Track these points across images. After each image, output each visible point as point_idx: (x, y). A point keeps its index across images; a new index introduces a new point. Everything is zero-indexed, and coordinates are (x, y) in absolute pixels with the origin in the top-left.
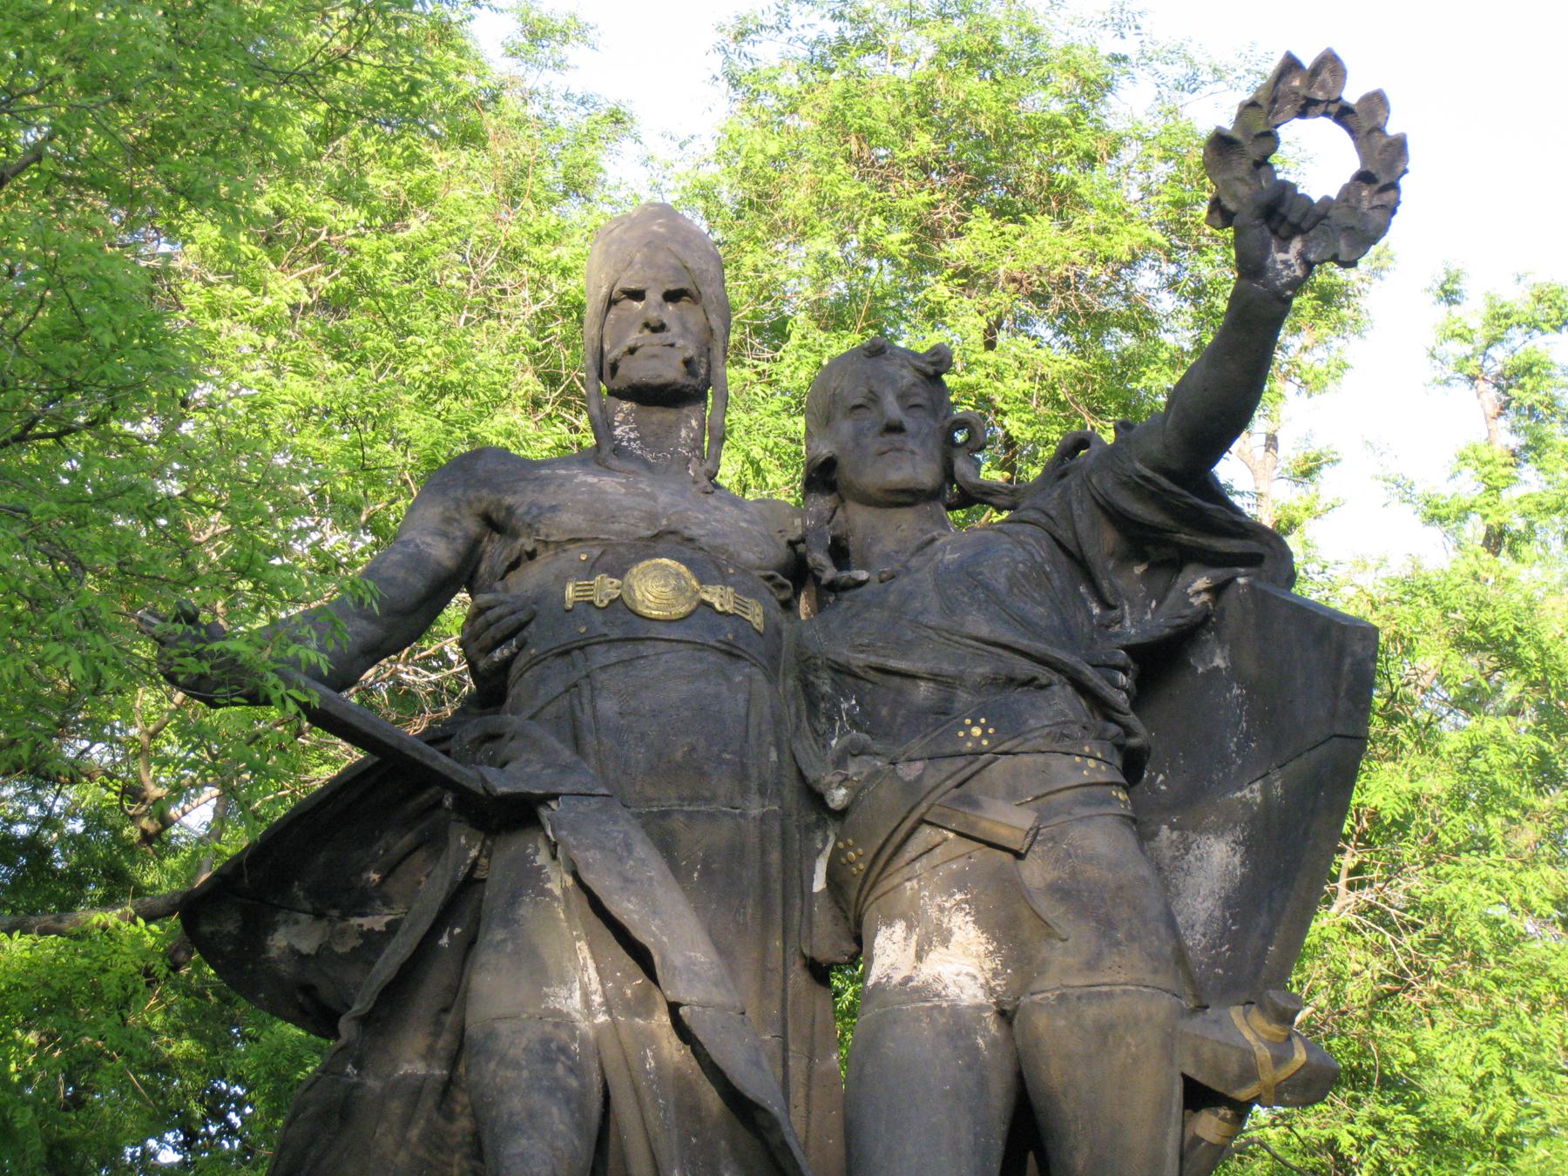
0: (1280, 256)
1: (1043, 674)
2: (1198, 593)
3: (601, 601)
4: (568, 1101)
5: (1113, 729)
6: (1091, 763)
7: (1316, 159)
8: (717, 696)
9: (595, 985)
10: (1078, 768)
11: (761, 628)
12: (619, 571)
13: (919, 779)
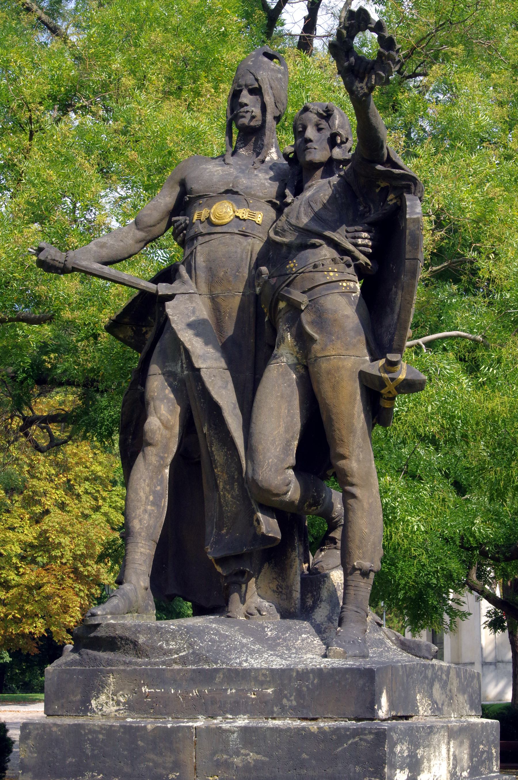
0: (361, 85)
1: (107, 270)
2: (391, 200)
3: (203, 218)
4: (168, 402)
5: (347, 258)
6: (331, 274)
7: (367, 43)
8: (236, 252)
9: (184, 361)
10: (325, 276)
11: (260, 222)
12: (210, 207)
13: (275, 283)
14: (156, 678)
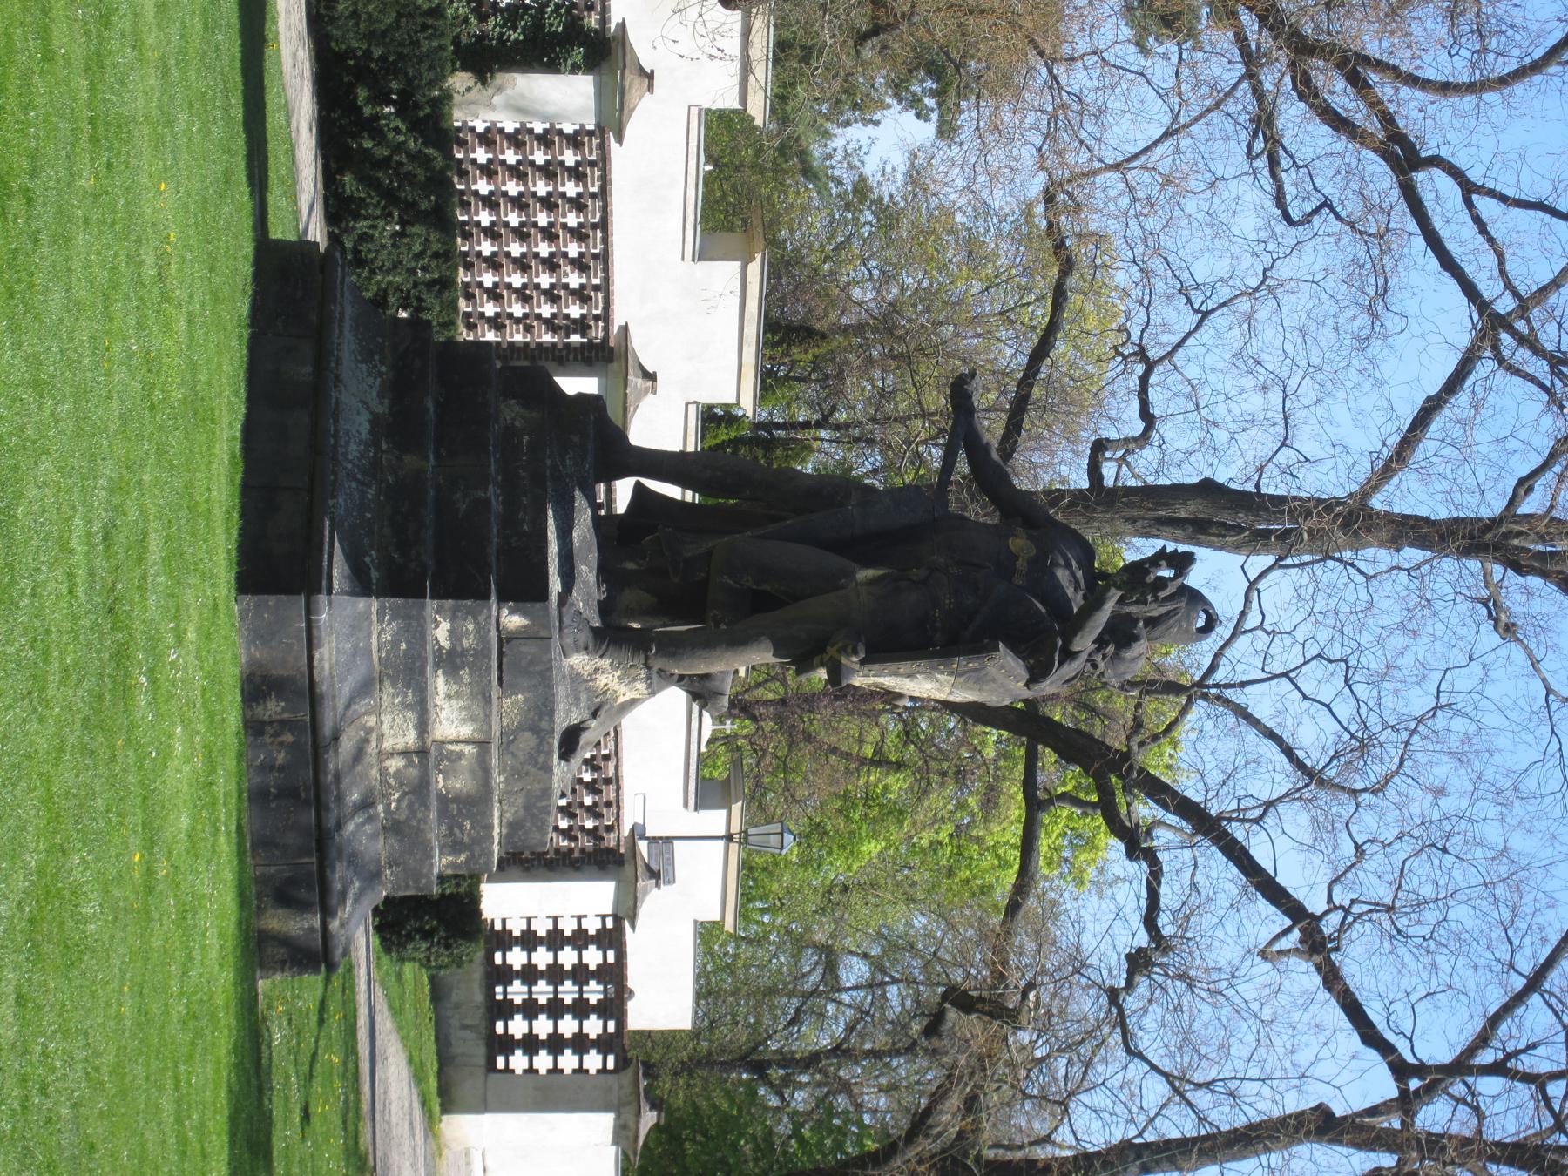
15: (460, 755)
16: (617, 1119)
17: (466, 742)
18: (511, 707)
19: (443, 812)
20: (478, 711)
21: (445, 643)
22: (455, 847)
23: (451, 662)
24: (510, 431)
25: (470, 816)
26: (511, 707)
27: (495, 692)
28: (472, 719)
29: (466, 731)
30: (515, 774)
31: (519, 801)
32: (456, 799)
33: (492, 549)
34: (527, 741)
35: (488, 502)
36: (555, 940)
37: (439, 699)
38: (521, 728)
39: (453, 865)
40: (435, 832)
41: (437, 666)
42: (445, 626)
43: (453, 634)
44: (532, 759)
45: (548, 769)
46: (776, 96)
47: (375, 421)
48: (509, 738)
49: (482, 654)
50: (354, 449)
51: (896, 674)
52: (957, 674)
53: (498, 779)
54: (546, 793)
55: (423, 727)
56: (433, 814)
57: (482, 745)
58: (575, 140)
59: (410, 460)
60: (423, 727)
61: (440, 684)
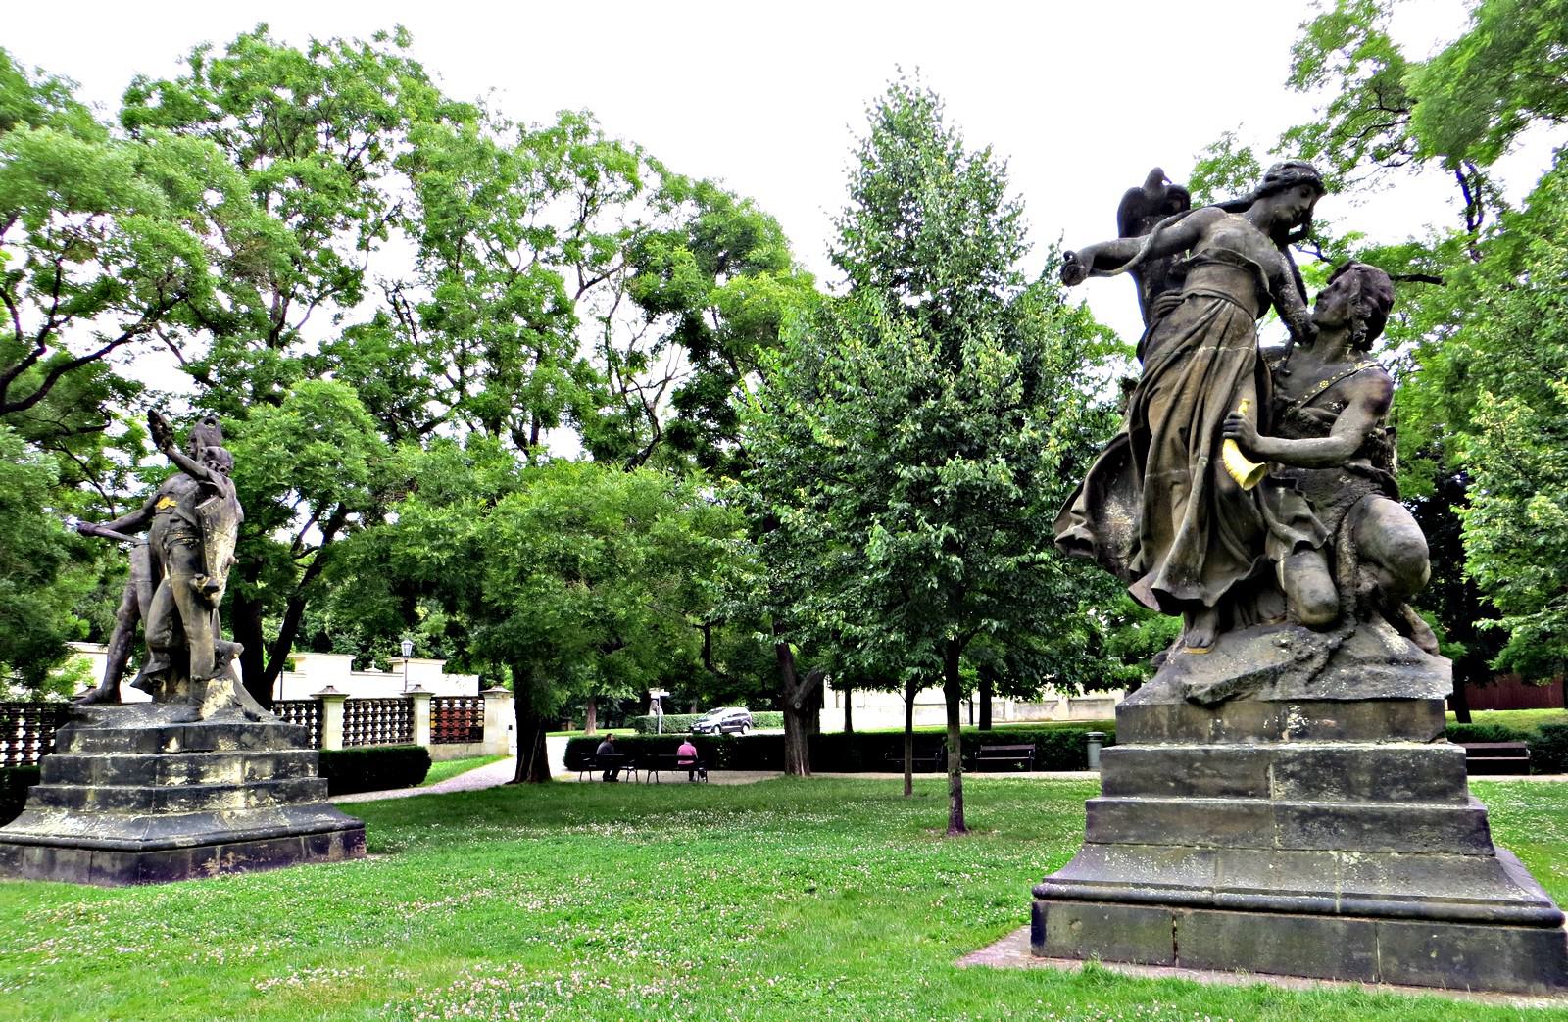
14: (92, 734)
15: (251, 770)
16: (818, 727)
17: (243, 767)
18: (225, 745)
19: (284, 776)
20: (225, 762)
21: (184, 778)
22: (304, 770)
23: (195, 775)
24: (85, 748)
25: (287, 763)
26: (225, 745)
27: (215, 753)
28: (230, 764)
29: (237, 766)
30: (265, 742)
31: (280, 740)
32: (277, 770)
33: (134, 756)
34: (246, 738)
35: (113, 759)
36: (346, 726)
37: (218, 780)
38: (238, 740)
39: (314, 770)
40: (296, 779)
41: (197, 782)
42: (173, 779)
43: (179, 774)
44: (257, 735)
45: (263, 728)
46: (1050, 789)
47: (70, 816)
48: (243, 746)
49: (191, 760)
50: (81, 826)
51: (213, 561)
52: (213, 530)
53: (267, 751)
54: (276, 728)
55: (233, 788)
56: (284, 781)
57: (247, 758)
58: (347, 709)
59: (90, 798)
60: (233, 788)
61: (208, 781)
